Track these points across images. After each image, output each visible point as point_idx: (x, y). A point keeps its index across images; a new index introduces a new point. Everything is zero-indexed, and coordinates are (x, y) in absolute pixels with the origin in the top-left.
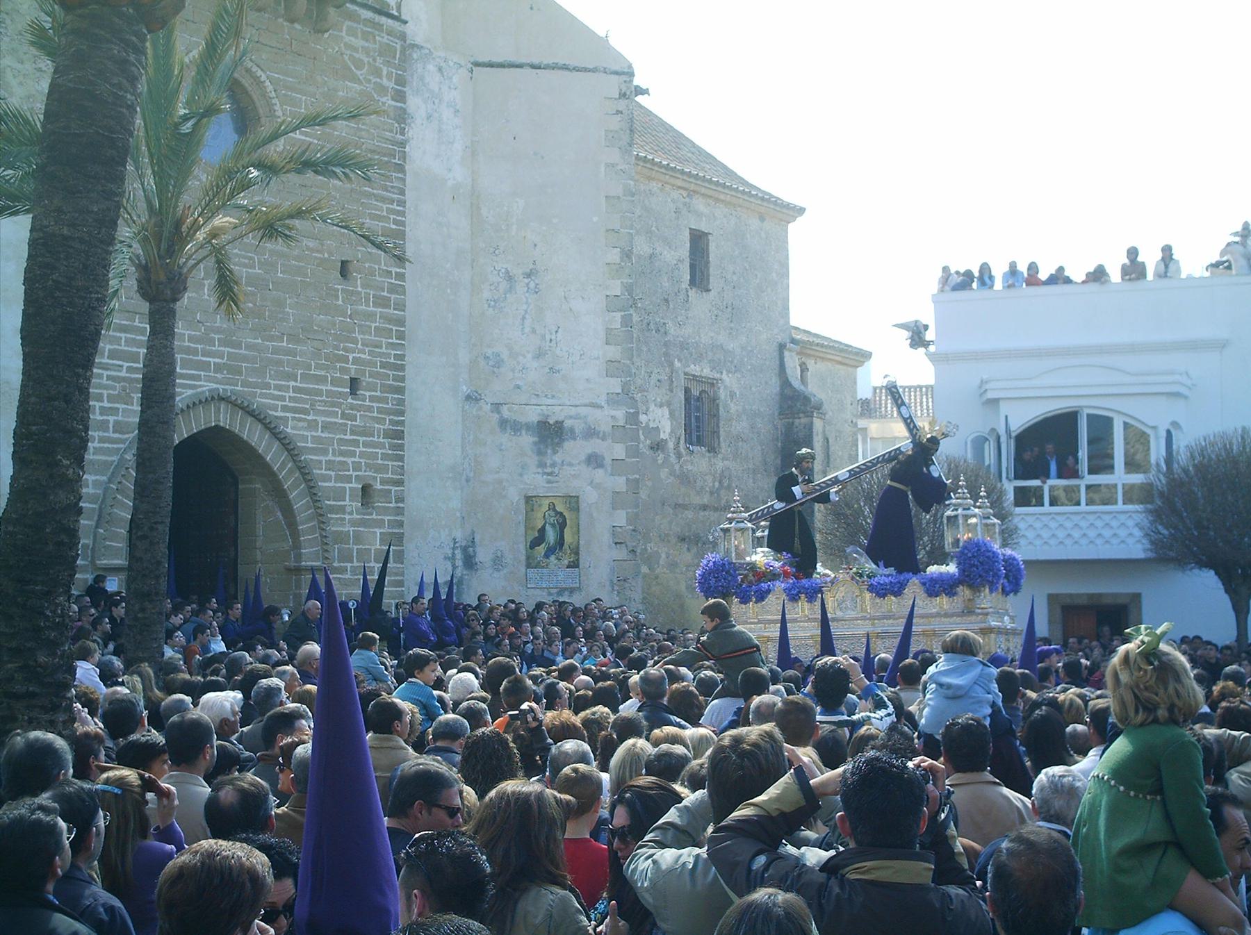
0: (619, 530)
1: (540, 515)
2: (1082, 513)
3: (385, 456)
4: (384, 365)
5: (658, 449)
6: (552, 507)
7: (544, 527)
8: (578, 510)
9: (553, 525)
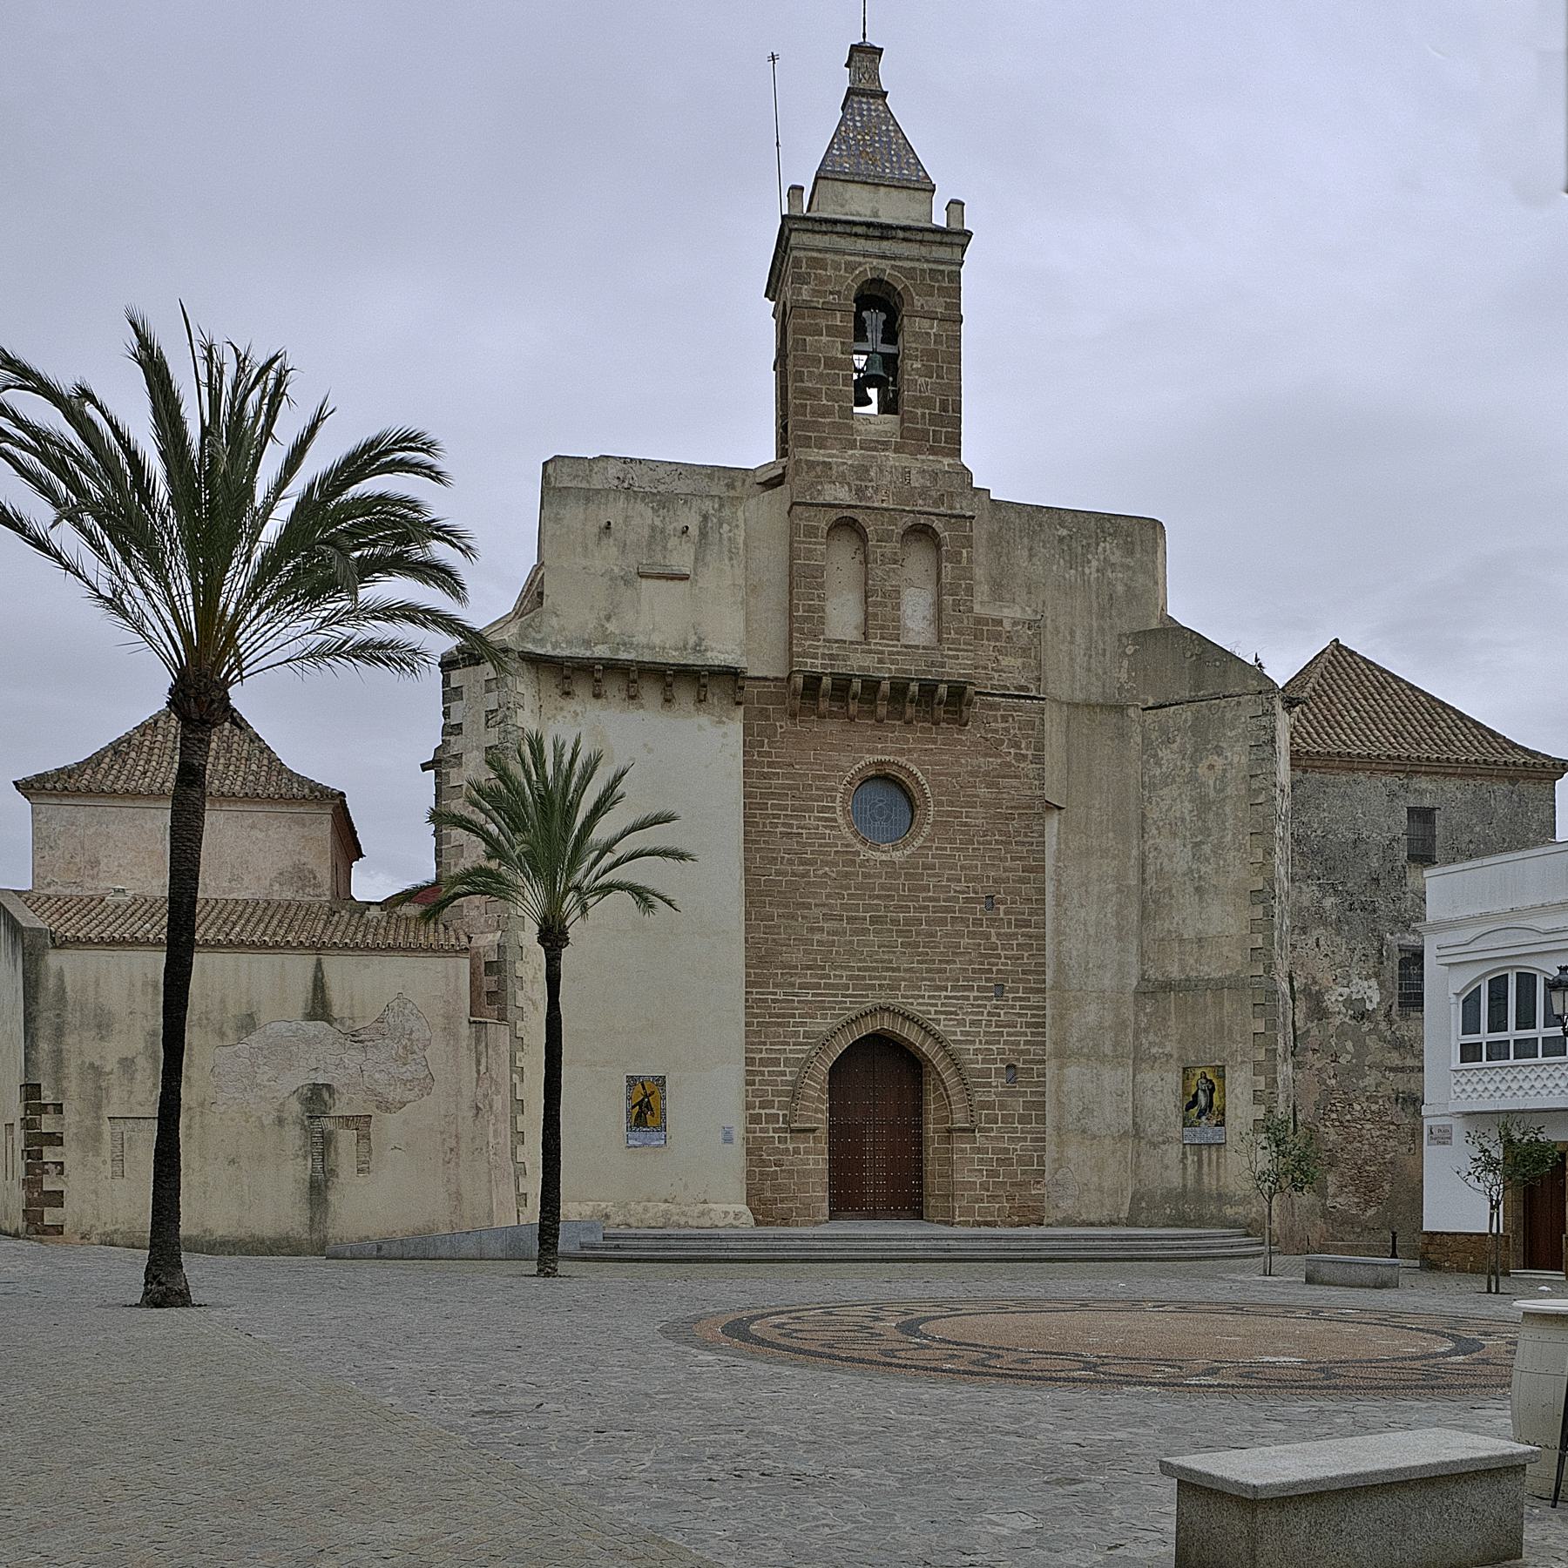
0: (1259, 1093)
1: (1194, 1083)
2: (1483, 1069)
3: (1026, 1043)
4: (1024, 972)
5: (1362, 1019)
6: (1204, 1076)
7: (1197, 1092)
8: (1224, 1077)
9: (1204, 1091)
